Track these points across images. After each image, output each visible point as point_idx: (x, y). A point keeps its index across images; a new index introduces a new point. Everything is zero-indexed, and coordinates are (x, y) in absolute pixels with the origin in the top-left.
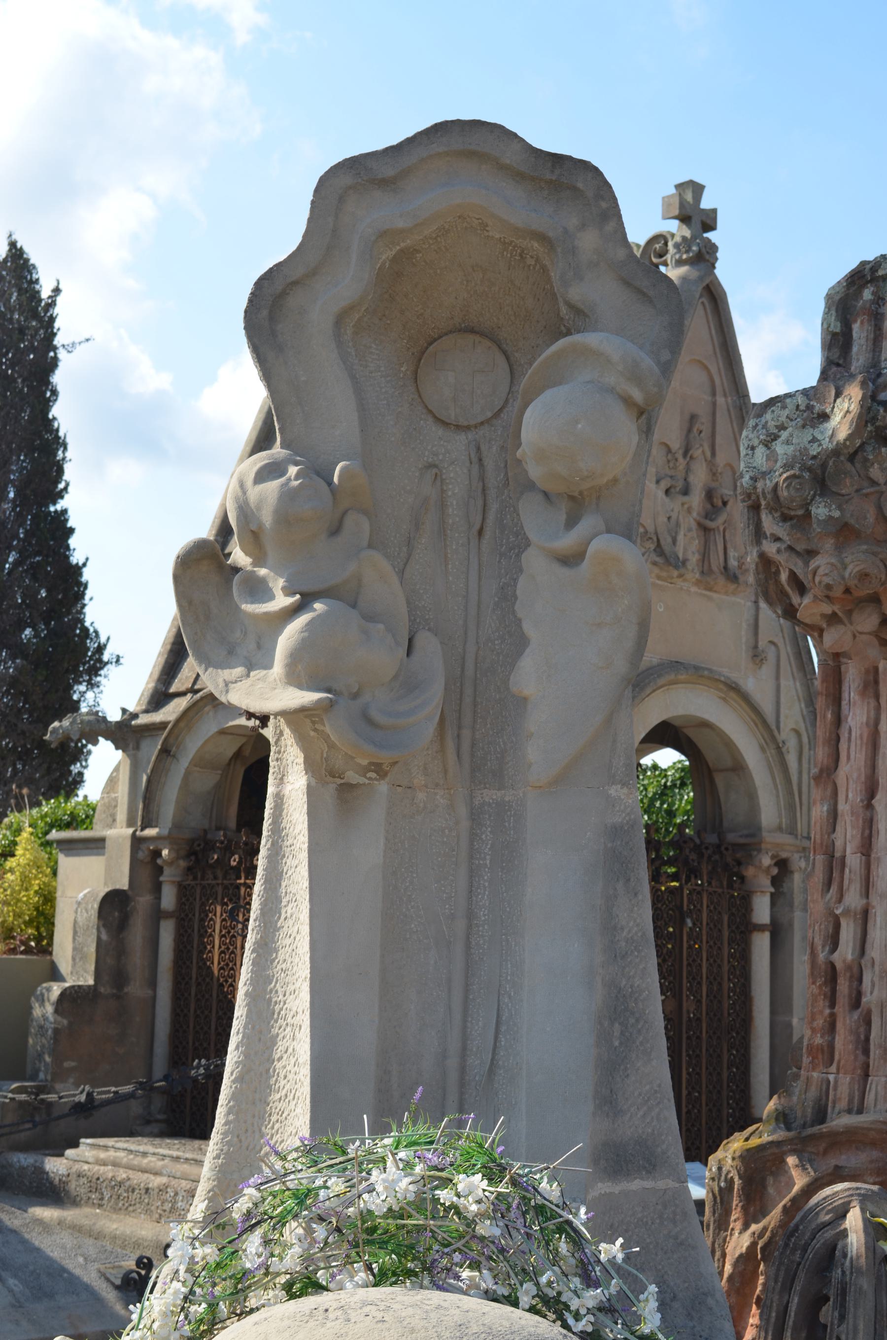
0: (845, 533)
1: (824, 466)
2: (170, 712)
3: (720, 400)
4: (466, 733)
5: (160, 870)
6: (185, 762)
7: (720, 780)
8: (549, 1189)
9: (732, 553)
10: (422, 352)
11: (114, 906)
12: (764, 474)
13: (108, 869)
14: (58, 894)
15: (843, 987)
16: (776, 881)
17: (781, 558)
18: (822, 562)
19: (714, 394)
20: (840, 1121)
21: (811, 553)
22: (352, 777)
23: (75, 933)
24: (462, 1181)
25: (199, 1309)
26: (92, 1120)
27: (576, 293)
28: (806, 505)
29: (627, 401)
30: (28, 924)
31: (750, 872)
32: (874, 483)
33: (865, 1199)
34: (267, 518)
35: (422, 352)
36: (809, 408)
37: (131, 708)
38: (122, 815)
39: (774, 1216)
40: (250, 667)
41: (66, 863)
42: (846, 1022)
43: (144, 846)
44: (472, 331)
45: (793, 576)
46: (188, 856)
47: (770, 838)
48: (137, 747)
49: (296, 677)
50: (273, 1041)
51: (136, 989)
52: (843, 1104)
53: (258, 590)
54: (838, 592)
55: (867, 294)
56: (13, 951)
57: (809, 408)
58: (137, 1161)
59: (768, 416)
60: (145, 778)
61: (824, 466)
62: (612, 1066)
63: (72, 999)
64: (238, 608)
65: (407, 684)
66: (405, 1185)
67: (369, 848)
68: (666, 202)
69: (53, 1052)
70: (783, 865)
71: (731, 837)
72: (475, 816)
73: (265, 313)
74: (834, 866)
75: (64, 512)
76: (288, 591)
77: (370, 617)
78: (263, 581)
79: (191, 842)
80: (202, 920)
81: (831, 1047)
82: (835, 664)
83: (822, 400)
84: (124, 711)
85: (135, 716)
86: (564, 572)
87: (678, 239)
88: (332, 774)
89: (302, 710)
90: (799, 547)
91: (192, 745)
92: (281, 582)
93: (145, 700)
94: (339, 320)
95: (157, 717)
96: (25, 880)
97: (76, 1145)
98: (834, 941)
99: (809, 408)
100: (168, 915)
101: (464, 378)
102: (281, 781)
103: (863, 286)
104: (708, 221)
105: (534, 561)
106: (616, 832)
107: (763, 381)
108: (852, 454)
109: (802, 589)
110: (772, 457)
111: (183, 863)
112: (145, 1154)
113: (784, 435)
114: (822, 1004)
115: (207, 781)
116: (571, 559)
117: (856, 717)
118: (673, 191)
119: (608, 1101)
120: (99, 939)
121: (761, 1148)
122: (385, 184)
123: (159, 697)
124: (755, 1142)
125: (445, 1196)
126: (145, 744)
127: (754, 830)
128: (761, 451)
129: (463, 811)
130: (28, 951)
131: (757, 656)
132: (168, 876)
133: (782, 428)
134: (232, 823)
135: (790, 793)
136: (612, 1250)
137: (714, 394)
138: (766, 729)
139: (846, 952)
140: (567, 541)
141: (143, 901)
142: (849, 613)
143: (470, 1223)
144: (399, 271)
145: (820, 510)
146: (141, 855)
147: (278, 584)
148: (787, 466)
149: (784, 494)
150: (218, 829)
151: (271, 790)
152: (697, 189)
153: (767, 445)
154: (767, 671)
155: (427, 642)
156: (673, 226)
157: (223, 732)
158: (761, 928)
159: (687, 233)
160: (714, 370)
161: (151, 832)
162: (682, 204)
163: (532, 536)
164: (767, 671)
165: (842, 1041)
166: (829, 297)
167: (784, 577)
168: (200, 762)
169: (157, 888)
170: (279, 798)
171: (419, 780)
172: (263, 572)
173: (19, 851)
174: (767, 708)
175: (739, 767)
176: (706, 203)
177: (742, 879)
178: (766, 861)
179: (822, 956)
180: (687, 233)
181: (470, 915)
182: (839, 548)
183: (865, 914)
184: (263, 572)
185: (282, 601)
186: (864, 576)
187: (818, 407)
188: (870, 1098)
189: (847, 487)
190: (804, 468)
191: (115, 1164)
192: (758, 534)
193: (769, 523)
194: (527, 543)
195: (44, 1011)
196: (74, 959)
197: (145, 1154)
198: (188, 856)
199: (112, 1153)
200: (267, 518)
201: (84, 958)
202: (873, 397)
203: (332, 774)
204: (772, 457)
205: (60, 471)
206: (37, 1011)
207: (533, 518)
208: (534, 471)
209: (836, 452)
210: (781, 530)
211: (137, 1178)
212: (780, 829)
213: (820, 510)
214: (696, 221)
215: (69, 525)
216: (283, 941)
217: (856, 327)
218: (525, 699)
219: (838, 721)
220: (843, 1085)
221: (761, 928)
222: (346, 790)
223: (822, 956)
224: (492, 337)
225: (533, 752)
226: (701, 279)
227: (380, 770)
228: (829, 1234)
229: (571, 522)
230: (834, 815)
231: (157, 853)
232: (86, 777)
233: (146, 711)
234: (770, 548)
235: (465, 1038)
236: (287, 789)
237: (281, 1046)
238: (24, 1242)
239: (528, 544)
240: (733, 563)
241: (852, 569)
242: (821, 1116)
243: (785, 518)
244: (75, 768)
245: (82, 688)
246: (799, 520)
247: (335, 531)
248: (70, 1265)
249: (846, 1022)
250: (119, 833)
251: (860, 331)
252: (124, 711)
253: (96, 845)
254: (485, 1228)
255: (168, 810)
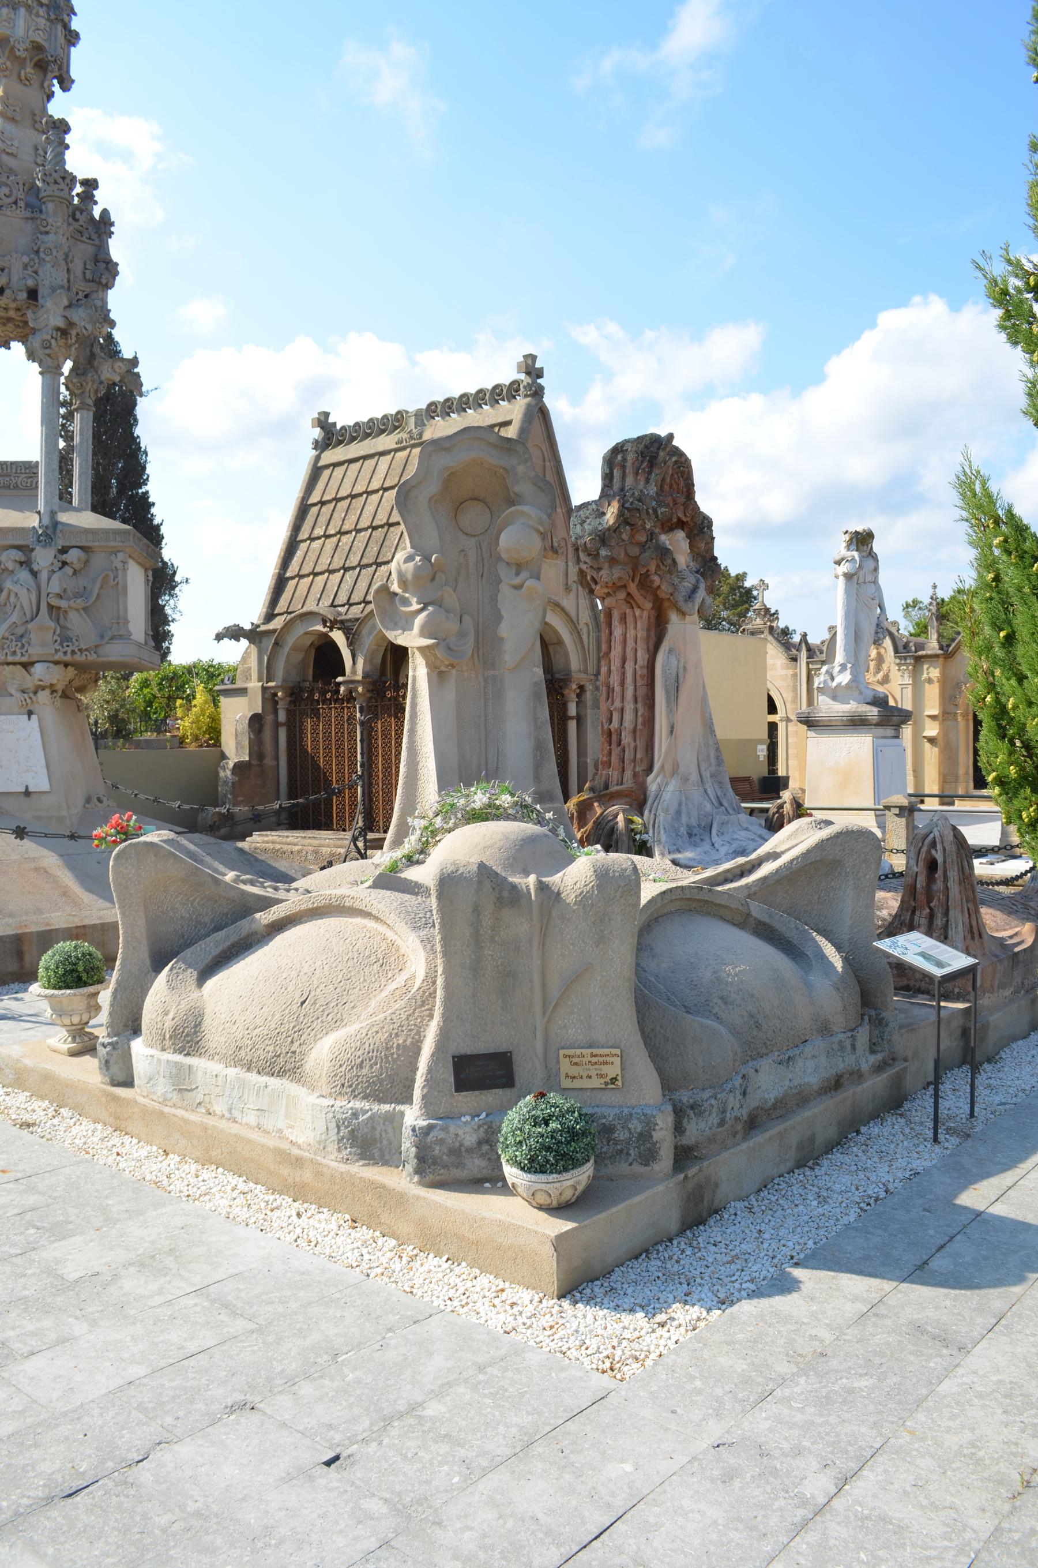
0: (613, 561)
1: (604, 534)
2: (277, 623)
3: (548, 464)
4: (481, 651)
5: (276, 703)
6: (287, 649)
7: (551, 649)
8: (529, 800)
9: (555, 540)
10: (458, 508)
11: (256, 721)
12: (581, 537)
13: (250, 703)
14: (222, 716)
15: (614, 737)
16: (578, 696)
17: (588, 571)
18: (604, 573)
19: (544, 461)
20: (613, 788)
21: (599, 569)
22: (443, 669)
23: (236, 735)
24: (503, 797)
25: (424, 839)
26: (259, 822)
27: (517, 489)
28: (597, 550)
29: (537, 531)
30: (205, 733)
31: (566, 692)
32: (623, 540)
33: (624, 811)
34: (409, 576)
35: (458, 508)
36: (598, 510)
37: (255, 622)
38: (255, 676)
39: (590, 825)
40: (404, 630)
41: (223, 701)
42: (616, 751)
43: (268, 691)
44: (475, 499)
45: (592, 578)
46: (291, 695)
47: (575, 675)
48: (260, 642)
49: (424, 633)
50: (418, 763)
51: (269, 761)
52: (615, 782)
53: (406, 602)
54: (610, 584)
55: (619, 457)
56: (201, 746)
57: (598, 510)
58: (284, 840)
59: (581, 513)
60: (266, 658)
61: (604, 534)
62: (538, 766)
63: (239, 767)
64: (397, 608)
65: (462, 634)
66: (485, 800)
67: (450, 694)
68: (519, 365)
69: (232, 793)
70: (581, 688)
71: (557, 676)
72: (486, 680)
73: (402, 498)
74: (610, 690)
75: (147, 492)
76: (418, 603)
77: (447, 611)
78: (407, 599)
79: (293, 688)
80: (300, 726)
81: (610, 761)
82: (609, 613)
83: (603, 507)
84: (252, 624)
85: (258, 626)
86: (516, 592)
87: (525, 383)
88: (436, 668)
89: (428, 647)
90: (595, 566)
91: (291, 640)
92: (415, 600)
93: (262, 617)
94: (430, 500)
95: (271, 626)
96: (203, 710)
97: (251, 835)
98: (610, 721)
99: (596, 509)
100: (283, 725)
101: (474, 517)
102: (415, 670)
103: (618, 454)
104: (540, 374)
105: (504, 588)
106: (536, 684)
107: (577, 498)
108: (615, 529)
109: (596, 583)
110: (583, 530)
111: (288, 699)
112: (287, 837)
113: (588, 521)
114: (606, 745)
115: (299, 657)
116: (518, 587)
117: (618, 632)
118: (522, 359)
119: (537, 779)
120: (250, 738)
121: (584, 800)
122: (446, 449)
123: (270, 616)
124: (582, 799)
125: (497, 802)
126: (265, 640)
127: (568, 673)
128: (579, 526)
129: (481, 679)
130: (209, 746)
131: (567, 588)
132: (281, 705)
133: (587, 518)
134: (311, 678)
135: (583, 647)
136: (549, 815)
137: (544, 461)
138: (572, 623)
139: (615, 724)
140: (517, 581)
141: (269, 718)
142: (615, 592)
143: (505, 809)
144: (451, 479)
145: (603, 552)
146: (267, 696)
147: (414, 600)
148: (590, 535)
149: (589, 546)
150: (304, 681)
151: (410, 674)
152: (534, 358)
153: (581, 524)
154: (572, 595)
155: (467, 618)
156: (522, 376)
157: (306, 633)
158: (572, 718)
159: (530, 381)
160: (544, 450)
161: (272, 684)
162: (527, 366)
163: (503, 578)
164: (572, 595)
165: (614, 758)
166: (604, 458)
167: (589, 578)
168: (295, 648)
169: (276, 712)
170: (414, 677)
171: (465, 668)
172: (407, 595)
173: (198, 696)
174: (573, 614)
175: (560, 642)
176: (537, 365)
177: (563, 695)
178: (574, 686)
179: (606, 727)
180: (530, 381)
181: (486, 716)
182: (611, 567)
183: (622, 709)
184: (407, 595)
185: (415, 607)
186: (620, 578)
187: (601, 510)
188: (625, 779)
189: (613, 543)
190: (597, 535)
191: (273, 842)
192: (578, 560)
193: (582, 556)
194: (501, 581)
195: (226, 773)
196: (235, 747)
197: (287, 837)
198: (291, 695)
199: (270, 838)
200: (409, 576)
201: (242, 747)
202: (623, 506)
203: (436, 668)
204: (583, 530)
205: (144, 468)
206: (222, 774)
207: (503, 572)
208: (504, 556)
209: (609, 529)
210: (587, 559)
211: (285, 847)
212: (580, 671)
213: (603, 552)
214: (534, 374)
215: (150, 500)
216: (419, 728)
217: (615, 471)
218: (503, 638)
219: (611, 633)
220: (614, 775)
221: (572, 718)
222: (441, 673)
223: (606, 727)
224: (483, 501)
225: (507, 657)
226: (537, 404)
227: (453, 666)
228: (612, 823)
229: (518, 574)
230: (610, 671)
231: (276, 695)
232: (171, 650)
233: (263, 624)
234: (584, 567)
235: (486, 757)
236: (417, 674)
237: (421, 765)
238: (269, 865)
239: (501, 581)
240: (556, 544)
241: (616, 576)
242: (606, 787)
243: (589, 555)
244: (165, 645)
245: (167, 598)
246: (595, 556)
247: (433, 579)
248: (290, 873)
249: (616, 751)
250: (254, 685)
251: (617, 473)
252: (252, 624)
253: (243, 691)
254: (510, 811)
255: (280, 672)
